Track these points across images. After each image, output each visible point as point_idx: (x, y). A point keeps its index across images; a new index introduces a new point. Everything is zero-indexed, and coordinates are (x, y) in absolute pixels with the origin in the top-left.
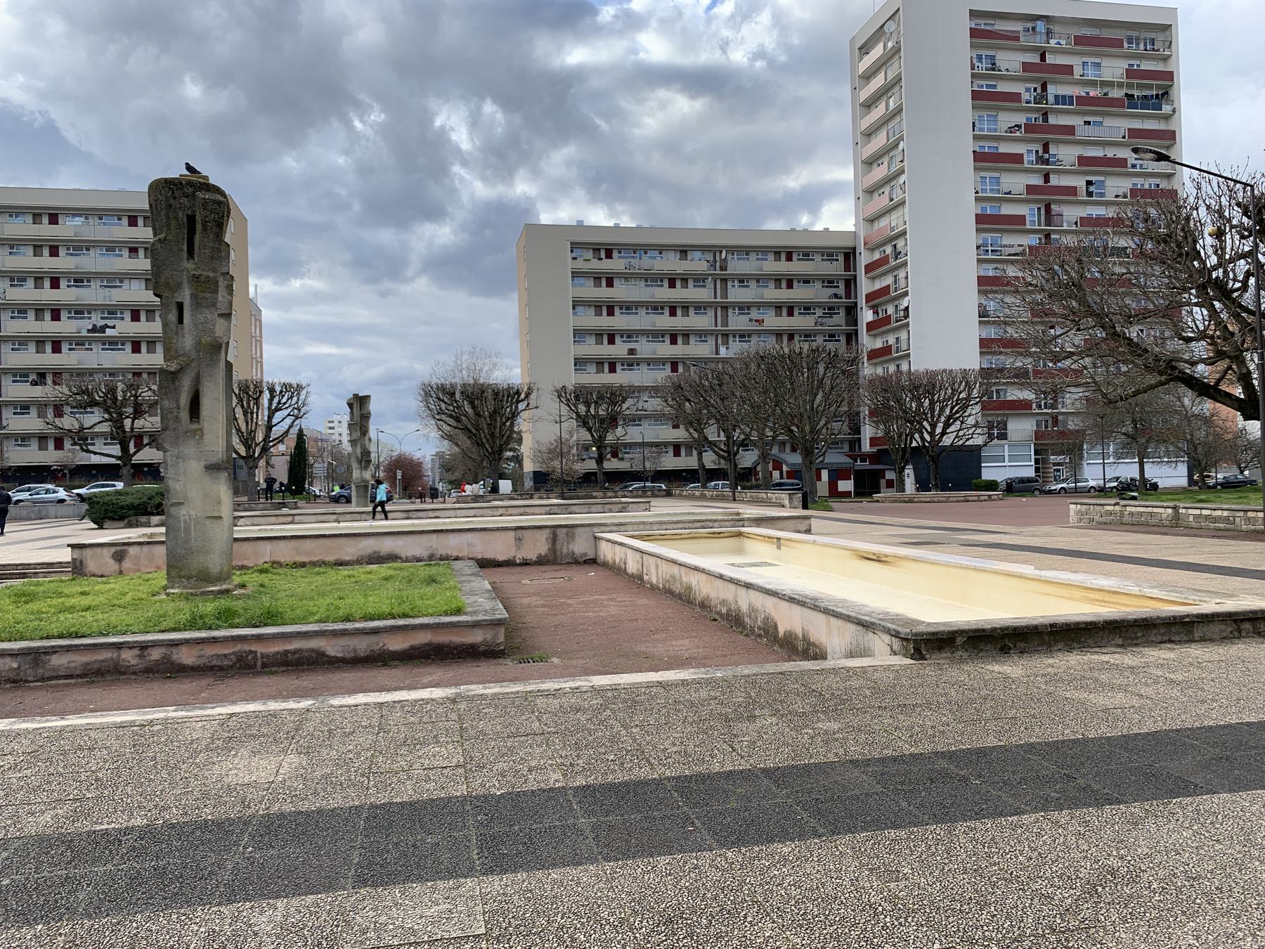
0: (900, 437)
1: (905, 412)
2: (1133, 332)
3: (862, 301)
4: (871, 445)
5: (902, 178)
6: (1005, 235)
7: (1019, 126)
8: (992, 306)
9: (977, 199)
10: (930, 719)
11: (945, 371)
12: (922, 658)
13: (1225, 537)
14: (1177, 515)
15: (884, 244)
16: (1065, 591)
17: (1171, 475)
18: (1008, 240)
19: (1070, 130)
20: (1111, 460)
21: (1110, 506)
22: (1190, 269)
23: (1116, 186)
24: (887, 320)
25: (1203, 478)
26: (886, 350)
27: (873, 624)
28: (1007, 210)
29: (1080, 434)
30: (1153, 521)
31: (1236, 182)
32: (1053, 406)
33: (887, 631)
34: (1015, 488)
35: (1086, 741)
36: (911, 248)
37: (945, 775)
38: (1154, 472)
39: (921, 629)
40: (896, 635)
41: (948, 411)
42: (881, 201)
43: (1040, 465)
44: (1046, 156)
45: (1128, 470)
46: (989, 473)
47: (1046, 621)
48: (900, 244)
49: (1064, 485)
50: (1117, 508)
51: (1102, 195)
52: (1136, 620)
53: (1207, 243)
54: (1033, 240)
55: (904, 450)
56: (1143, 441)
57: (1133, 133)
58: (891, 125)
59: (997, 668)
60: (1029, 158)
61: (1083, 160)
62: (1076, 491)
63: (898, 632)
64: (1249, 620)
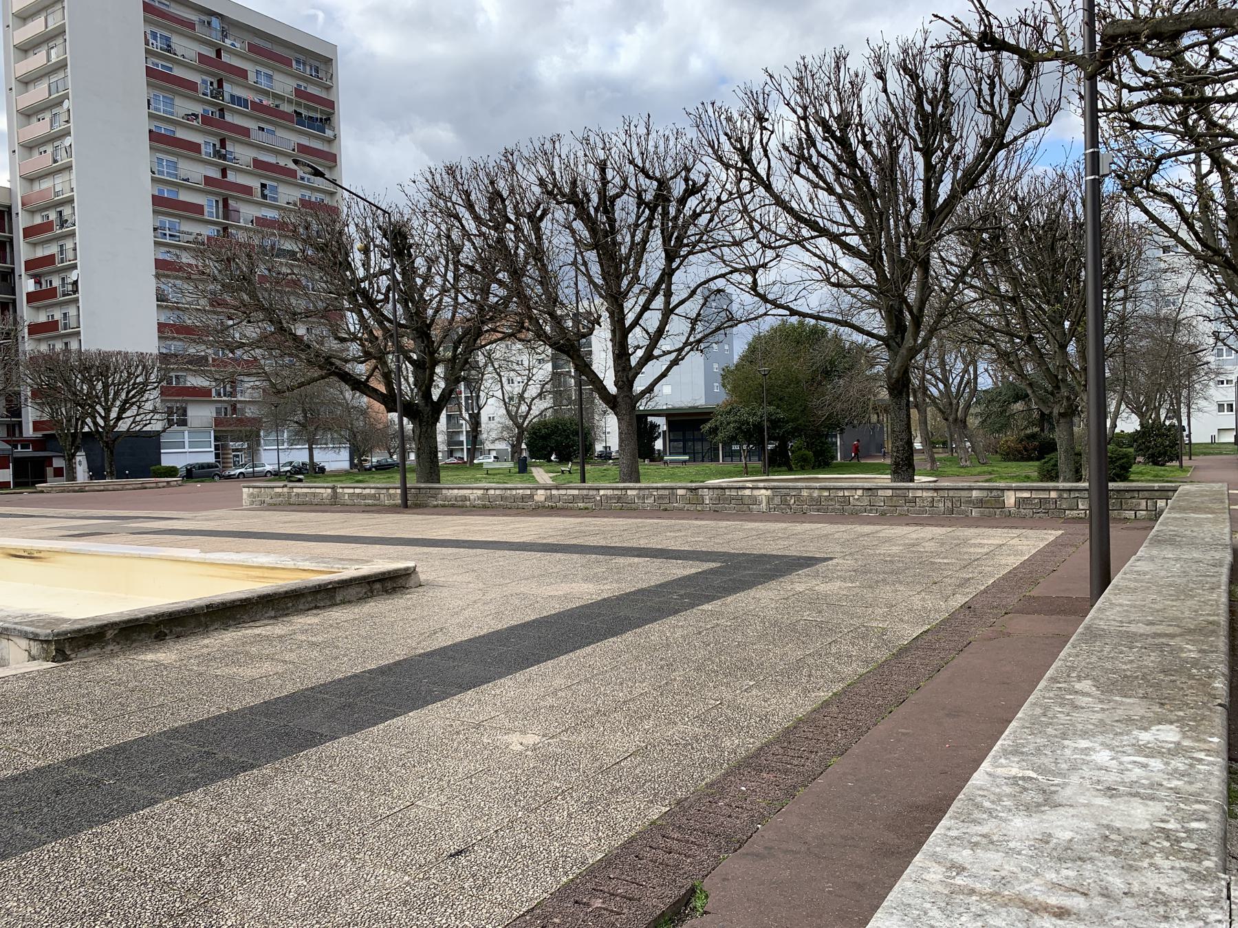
0: (69, 421)
1: (75, 394)
2: (301, 331)
3: (20, 268)
4: (35, 430)
5: (68, 141)
6: (183, 222)
7: (197, 116)
8: (168, 290)
9: (153, 180)
10: (66, 724)
11: (119, 353)
12: (67, 658)
13: (372, 512)
14: (335, 495)
15: (47, 208)
16: (225, 572)
17: (335, 459)
18: (186, 227)
19: (246, 132)
20: (286, 446)
21: (280, 488)
22: (343, 279)
23: (288, 194)
24: (52, 292)
25: (361, 461)
26: (51, 326)
27: (7, 629)
28: (185, 196)
29: (256, 421)
30: (316, 501)
31: (378, 208)
32: (231, 394)
33: (25, 635)
34: (193, 474)
35: (230, 714)
36: (79, 216)
37: (75, 782)
38: (320, 457)
39: (65, 627)
40: (34, 638)
41: (123, 396)
42: (41, 161)
43: (220, 451)
44: (223, 151)
45: (300, 456)
46: (168, 459)
47: (202, 603)
48: (67, 211)
49: (243, 470)
50: (285, 490)
51: (276, 199)
52: (286, 592)
53: (357, 257)
54: (207, 231)
55: (74, 436)
56: (312, 428)
57: (303, 149)
58: (53, 79)
59: (150, 656)
60: (207, 150)
61: (258, 163)
62: (254, 476)
63: (37, 635)
64: (379, 580)
